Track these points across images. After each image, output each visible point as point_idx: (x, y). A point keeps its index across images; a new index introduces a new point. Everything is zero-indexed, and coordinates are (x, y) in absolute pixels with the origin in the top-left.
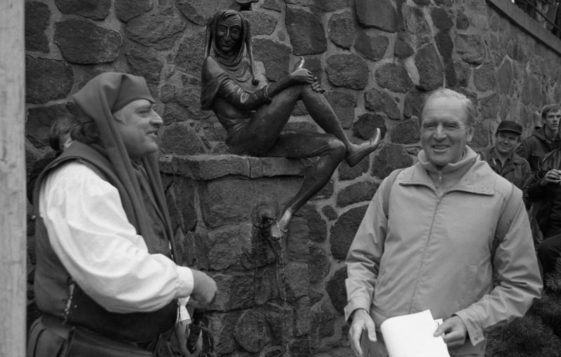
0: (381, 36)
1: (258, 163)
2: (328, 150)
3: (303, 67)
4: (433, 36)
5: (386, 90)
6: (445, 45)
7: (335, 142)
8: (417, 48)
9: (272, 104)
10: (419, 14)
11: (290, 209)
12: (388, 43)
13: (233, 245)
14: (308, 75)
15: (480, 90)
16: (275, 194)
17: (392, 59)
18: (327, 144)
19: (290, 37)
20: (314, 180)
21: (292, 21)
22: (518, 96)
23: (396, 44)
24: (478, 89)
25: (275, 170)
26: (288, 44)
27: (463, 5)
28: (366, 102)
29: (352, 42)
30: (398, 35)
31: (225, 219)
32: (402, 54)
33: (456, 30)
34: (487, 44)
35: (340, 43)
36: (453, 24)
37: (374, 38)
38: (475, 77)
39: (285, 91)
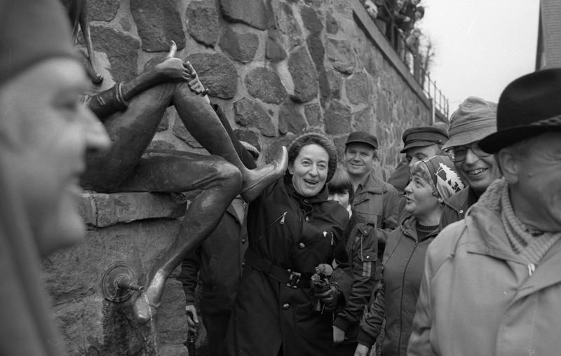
0: (249, 34)
1: (109, 202)
2: (217, 180)
3: (175, 56)
4: (305, 38)
5: (258, 100)
6: (317, 50)
7: (226, 168)
8: (289, 51)
9: (129, 111)
10: (289, 12)
11: (161, 270)
12: (258, 44)
13: (74, 335)
14: (183, 67)
15: (353, 103)
16: (136, 249)
17: (263, 63)
18: (216, 170)
19: (138, 27)
20: (199, 225)
21: (140, 6)
22: (374, 112)
23: (266, 44)
24: (351, 101)
25: (134, 212)
26: (135, 35)
27: (331, 6)
28: (237, 115)
29: (216, 38)
30: (269, 34)
31: (59, 296)
32: (274, 57)
33: (327, 34)
34: (356, 52)
35: (202, 38)
36: (322, 27)
37: (242, 35)
38: (346, 88)
39: (148, 91)
